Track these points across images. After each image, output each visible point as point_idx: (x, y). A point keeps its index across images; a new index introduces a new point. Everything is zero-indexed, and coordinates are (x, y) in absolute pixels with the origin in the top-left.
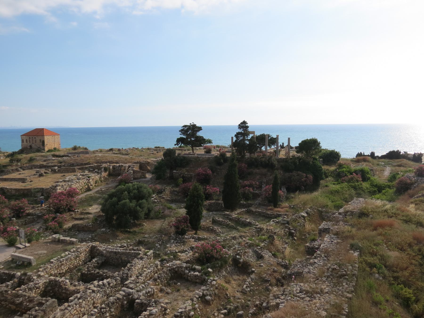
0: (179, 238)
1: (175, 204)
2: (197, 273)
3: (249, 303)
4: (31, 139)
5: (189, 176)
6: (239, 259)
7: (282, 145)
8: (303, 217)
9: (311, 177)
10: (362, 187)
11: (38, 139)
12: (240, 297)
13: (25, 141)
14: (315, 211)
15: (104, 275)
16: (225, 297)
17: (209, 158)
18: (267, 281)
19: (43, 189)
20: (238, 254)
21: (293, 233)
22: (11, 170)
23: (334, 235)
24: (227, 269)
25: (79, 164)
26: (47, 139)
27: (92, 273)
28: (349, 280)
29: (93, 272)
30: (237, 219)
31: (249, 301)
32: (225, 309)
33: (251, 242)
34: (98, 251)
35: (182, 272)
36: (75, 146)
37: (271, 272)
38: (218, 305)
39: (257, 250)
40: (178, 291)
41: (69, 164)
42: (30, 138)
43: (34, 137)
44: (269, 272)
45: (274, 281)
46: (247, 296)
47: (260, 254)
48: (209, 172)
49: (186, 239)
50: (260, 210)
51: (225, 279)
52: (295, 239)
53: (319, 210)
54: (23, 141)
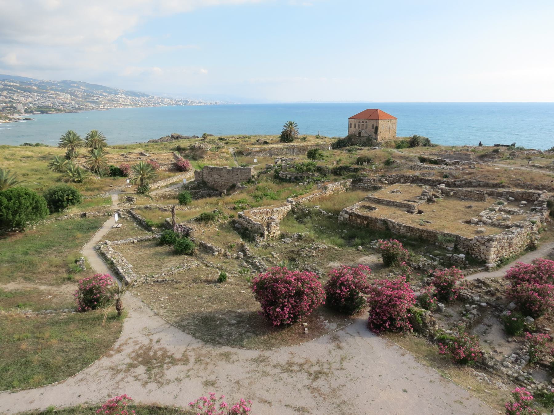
11: (370, 124)
13: (353, 126)
19: (458, 237)
22: (372, 181)
25: (482, 184)
26: (382, 124)
41: (463, 182)
42: (359, 122)
43: (364, 121)
54: (350, 126)
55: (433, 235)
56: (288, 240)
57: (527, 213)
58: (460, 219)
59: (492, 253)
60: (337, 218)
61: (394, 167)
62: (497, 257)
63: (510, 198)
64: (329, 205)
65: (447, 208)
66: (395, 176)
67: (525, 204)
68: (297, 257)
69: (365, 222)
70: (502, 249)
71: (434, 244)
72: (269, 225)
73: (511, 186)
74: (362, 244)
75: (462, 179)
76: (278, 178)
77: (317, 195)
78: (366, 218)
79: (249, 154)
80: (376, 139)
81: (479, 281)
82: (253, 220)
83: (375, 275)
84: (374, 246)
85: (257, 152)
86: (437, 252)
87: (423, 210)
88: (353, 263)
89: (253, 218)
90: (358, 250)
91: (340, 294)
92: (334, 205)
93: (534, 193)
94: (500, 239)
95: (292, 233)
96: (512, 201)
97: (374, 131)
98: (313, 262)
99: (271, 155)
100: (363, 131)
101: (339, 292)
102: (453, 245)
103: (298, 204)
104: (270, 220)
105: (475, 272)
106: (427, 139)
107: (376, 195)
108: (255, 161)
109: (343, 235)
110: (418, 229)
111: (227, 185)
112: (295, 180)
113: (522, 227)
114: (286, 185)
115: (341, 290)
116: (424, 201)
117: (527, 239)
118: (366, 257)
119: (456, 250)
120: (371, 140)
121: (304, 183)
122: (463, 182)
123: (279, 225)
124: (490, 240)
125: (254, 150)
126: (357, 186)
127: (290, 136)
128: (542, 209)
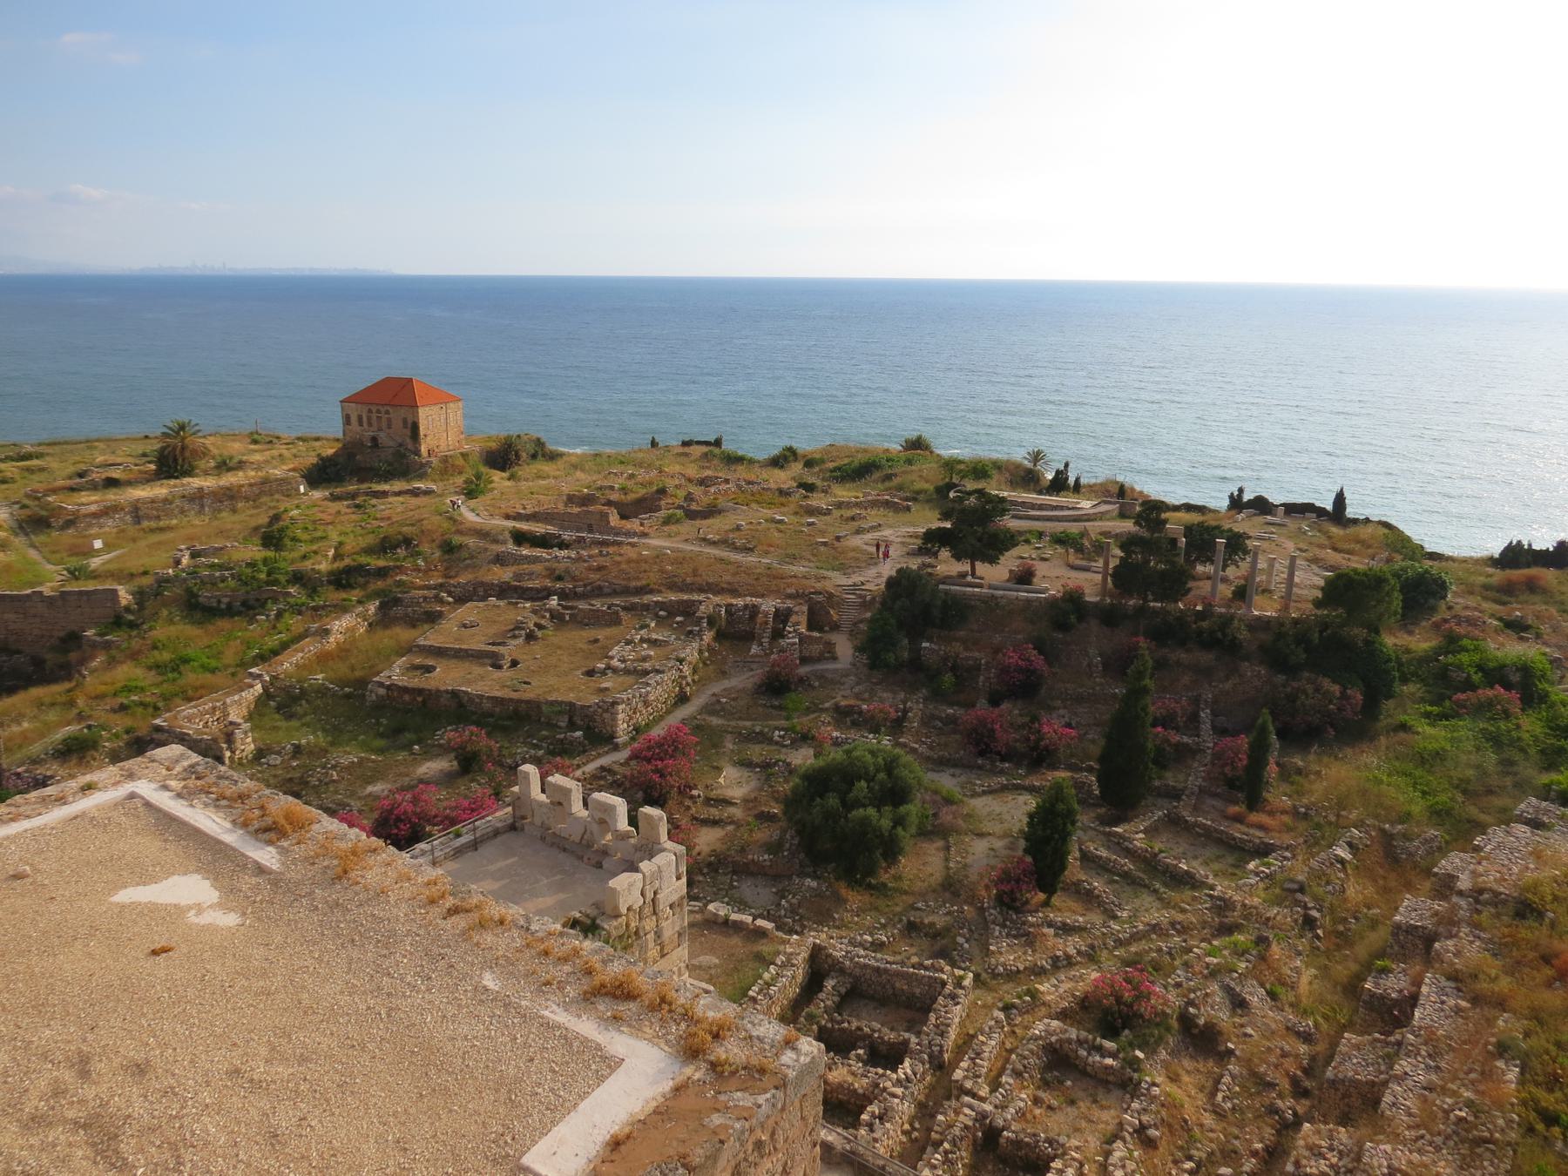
0: (1012, 921)
1: (953, 776)
2: (1109, 1061)
3: (1236, 1142)
4: (374, 416)
5: (971, 662)
6: (1195, 1015)
7: (1236, 493)
8: (1342, 861)
9: (1357, 695)
10: (1519, 739)
11: (397, 415)
12: (1214, 1127)
13: (354, 419)
14: (1373, 834)
15: (876, 1035)
16: (1182, 1127)
17: (1028, 601)
18: (1271, 1085)
19: (571, 705)
20: (1191, 1003)
21: (1316, 919)
22: (421, 600)
23: (1448, 979)
24: (1167, 1043)
27: (843, 1030)
28: (1498, 1153)
29: (846, 1025)
30: (1148, 855)
31: (1237, 1138)
32: (1190, 1158)
33: (1215, 961)
34: (830, 961)
35: (1070, 1054)
36: (509, 438)
37: (1278, 1059)
38: (1172, 1147)
39: (1232, 984)
40: (1072, 1102)
42: (370, 411)
43: (383, 409)
44: (1273, 1059)
45: (1285, 1085)
46: (1228, 1123)
47: (1239, 995)
48: (1038, 661)
49: (1032, 925)
50: (1209, 823)
51: (1167, 1069)
52: (1318, 937)
53: (1383, 831)
54: (347, 420)
55: (534, 705)
56: (275, 760)
57: (680, 640)
58: (578, 668)
59: (620, 722)
60: (364, 695)
61: (463, 557)
62: (629, 726)
63: (662, 613)
64: (342, 669)
65: (560, 648)
66: (466, 584)
67: (681, 622)
68: (302, 790)
69: (420, 699)
70: (635, 713)
71: (539, 720)
72: (230, 738)
73: (664, 590)
74: (419, 742)
75: (586, 582)
76: (197, 608)
77: (310, 651)
78: (420, 691)
79: (70, 523)
80: (417, 453)
81: (602, 768)
82: (191, 732)
83: (448, 793)
84: (442, 742)
85: (95, 515)
86: (544, 733)
87: (519, 657)
88: (407, 779)
89: (190, 729)
90: (414, 754)
91: (397, 835)
92: (353, 669)
93: (694, 601)
94: (628, 699)
95: (279, 743)
96: (663, 618)
97: (409, 433)
98: (336, 792)
99: (137, 519)
100: (382, 434)
101: (396, 831)
102: (566, 718)
103: (275, 678)
104: (231, 728)
105: (599, 756)
106: (538, 440)
107: (431, 637)
108: (98, 544)
109: (381, 729)
110: (511, 700)
111: (51, 637)
112: (242, 609)
113: (662, 672)
114: (223, 624)
115: (398, 828)
116: (520, 641)
117: (674, 688)
118: (429, 764)
119: (572, 726)
120: (404, 456)
121: (268, 616)
122: (589, 588)
123: (250, 734)
124: (614, 704)
125: (84, 510)
126: (392, 613)
127: (183, 460)
128: (701, 630)
